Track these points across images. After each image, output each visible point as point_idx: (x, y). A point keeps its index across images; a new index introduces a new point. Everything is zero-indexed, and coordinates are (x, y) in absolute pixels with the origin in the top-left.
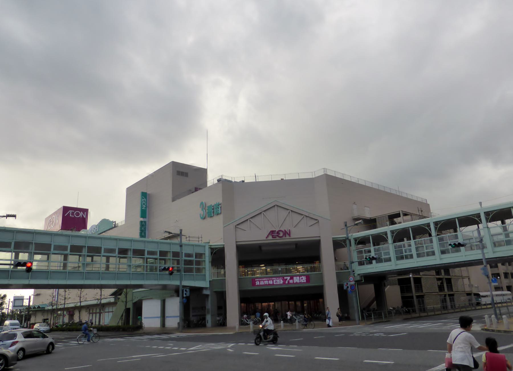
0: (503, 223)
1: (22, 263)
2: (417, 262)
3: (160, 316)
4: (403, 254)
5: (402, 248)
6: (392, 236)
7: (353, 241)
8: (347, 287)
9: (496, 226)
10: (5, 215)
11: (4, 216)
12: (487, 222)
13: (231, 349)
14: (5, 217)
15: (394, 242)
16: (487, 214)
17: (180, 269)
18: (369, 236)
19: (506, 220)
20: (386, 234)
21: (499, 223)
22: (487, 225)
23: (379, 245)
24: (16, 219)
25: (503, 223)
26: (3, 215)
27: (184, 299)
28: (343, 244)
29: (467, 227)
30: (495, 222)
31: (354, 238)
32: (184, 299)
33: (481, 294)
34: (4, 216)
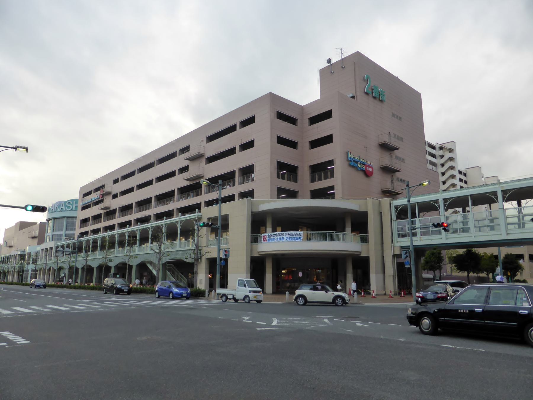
0: (519, 204)
1: (41, 208)
2: (475, 236)
3: (497, 248)
4: (406, 231)
5: (406, 225)
6: (396, 211)
7: (394, 209)
8: (405, 256)
9: (511, 206)
10: (14, 147)
11: (13, 148)
12: (504, 202)
13: (250, 320)
14: (14, 149)
15: (92, 252)
16: (504, 192)
17: (218, 227)
18: (414, 204)
19: (522, 200)
20: (437, 201)
21: (515, 203)
22: (503, 206)
23: (276, 232)
24: (27, 152)
25: (519, 204)
26: (11, 146)
27: (223, 261)
28: (448, 203)
29: (476, 206)
30: (510, 202)
31: (395, 206)
32: (223, 261)
33: (256, 302)
34: (13, 148)
